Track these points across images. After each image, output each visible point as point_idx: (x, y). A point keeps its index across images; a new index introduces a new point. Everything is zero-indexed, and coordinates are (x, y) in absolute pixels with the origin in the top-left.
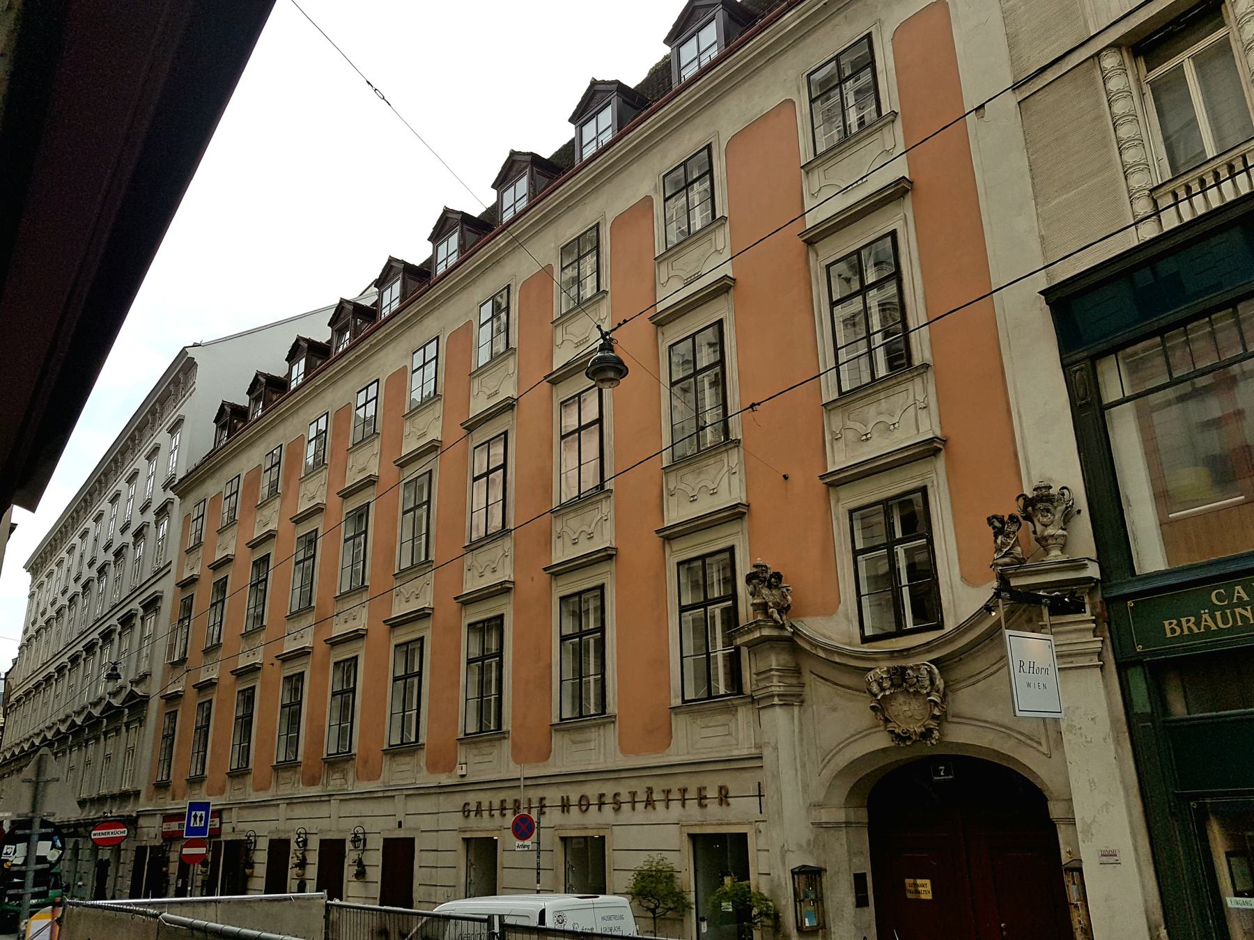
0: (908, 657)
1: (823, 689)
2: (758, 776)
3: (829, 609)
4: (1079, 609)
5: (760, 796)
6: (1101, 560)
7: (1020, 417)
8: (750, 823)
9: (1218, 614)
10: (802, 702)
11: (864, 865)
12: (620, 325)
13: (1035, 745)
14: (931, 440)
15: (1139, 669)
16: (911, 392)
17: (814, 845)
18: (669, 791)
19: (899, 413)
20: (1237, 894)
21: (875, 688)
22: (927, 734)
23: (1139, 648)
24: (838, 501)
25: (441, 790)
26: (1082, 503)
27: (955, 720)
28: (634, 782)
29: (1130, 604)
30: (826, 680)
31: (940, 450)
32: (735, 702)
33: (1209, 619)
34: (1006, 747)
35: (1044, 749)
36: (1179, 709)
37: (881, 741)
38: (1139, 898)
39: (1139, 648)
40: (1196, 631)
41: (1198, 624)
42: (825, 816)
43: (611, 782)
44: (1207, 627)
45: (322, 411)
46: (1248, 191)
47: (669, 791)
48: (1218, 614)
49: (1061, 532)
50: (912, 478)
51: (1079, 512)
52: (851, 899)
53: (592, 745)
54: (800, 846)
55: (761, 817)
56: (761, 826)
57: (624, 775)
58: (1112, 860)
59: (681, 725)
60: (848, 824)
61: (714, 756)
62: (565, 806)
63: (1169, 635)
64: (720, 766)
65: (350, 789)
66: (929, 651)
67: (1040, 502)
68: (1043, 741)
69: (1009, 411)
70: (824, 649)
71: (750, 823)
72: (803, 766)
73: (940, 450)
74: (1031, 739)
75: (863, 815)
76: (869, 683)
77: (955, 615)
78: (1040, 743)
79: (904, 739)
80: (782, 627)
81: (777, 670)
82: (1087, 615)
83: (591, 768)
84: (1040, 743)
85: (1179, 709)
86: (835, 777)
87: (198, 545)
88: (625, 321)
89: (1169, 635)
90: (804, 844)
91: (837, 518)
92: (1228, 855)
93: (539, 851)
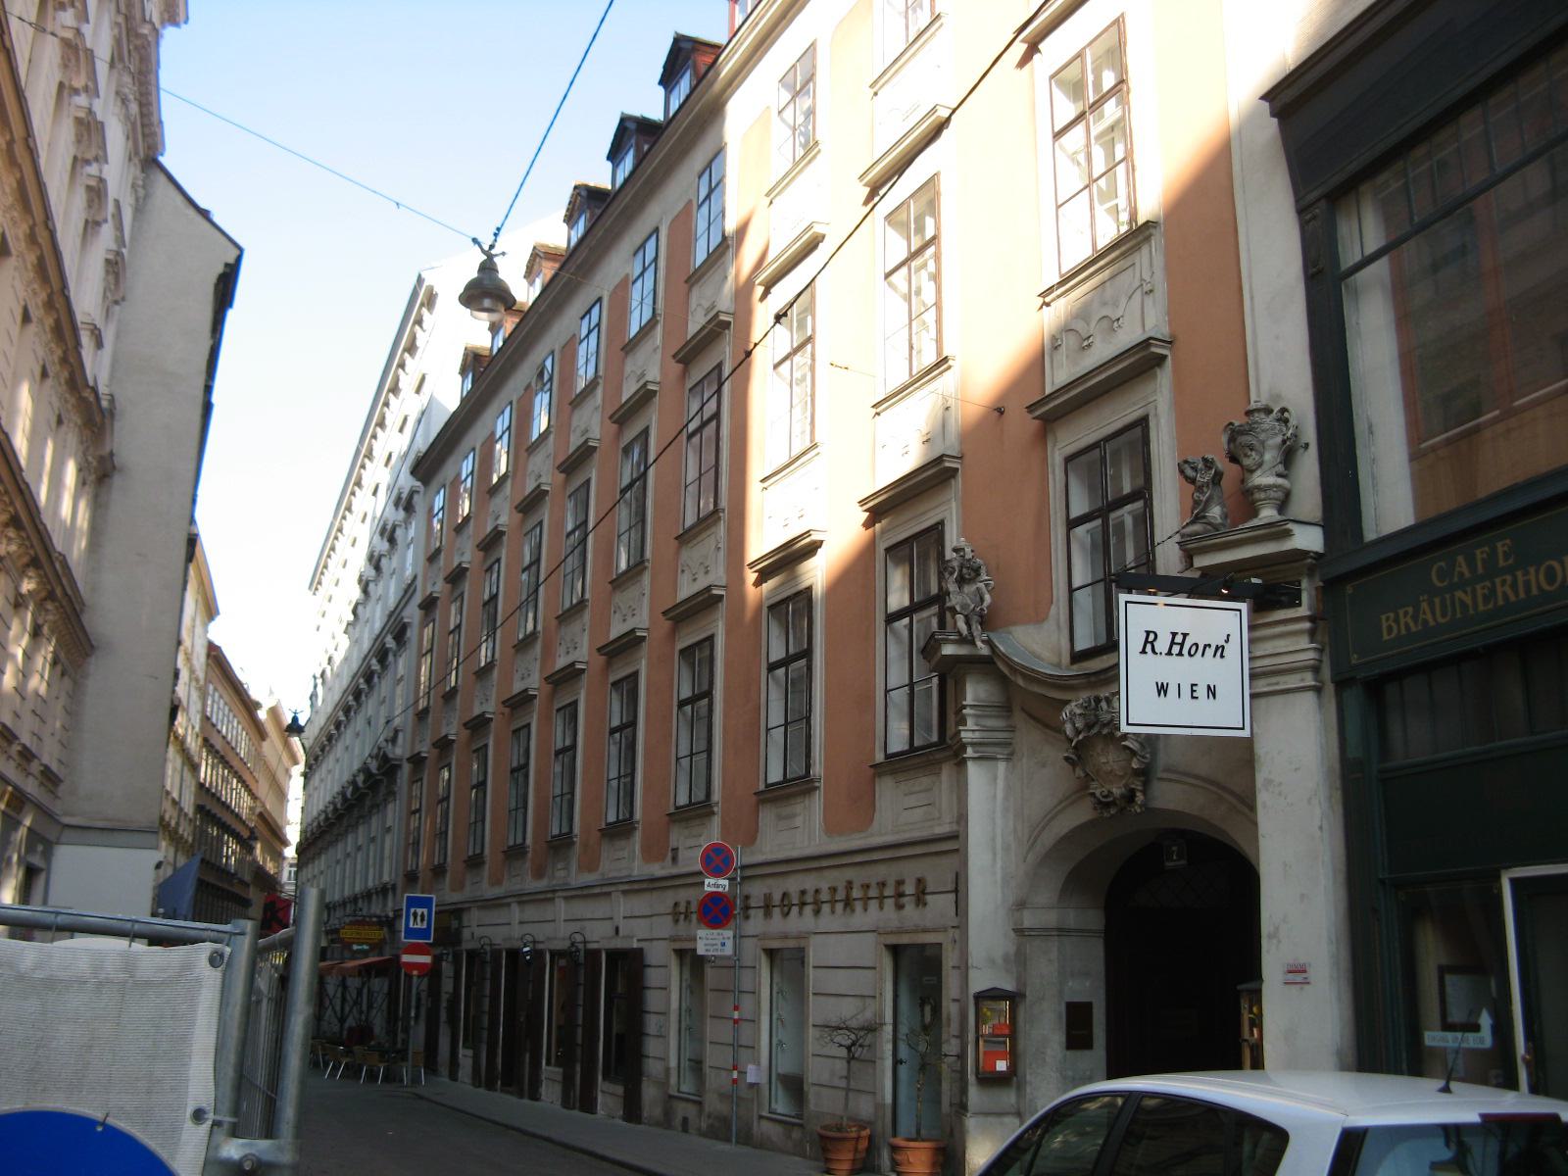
3: (1039, 618)
4: (1294, 601)
5: (956, 891)
6: (1327, 525)
7: (1252, 298)
9: (1437, 600)
11: (1090, 989)
12: (496, 235)
14: (1146, 343)
16: (1138, 265)
17: (1019, 961)
18: (868, 886)
19: (1124, 300)
20: (1448, 1027)
22: (1130, 797)
25: (653, 885)
26: (1310, 434)
28: (835, 873)
31: (1164, 357)
32: (937, 756)
33: (1428, 611)
39: (1355, 659)
40: (1414, 629)
41: (1415, 618)
42: (1029, 920)
43: (814, 875)
44: (1425, 622)
45: (547, 350)
47: (868, 886)
48: (1437, 600)
49: (1280, 481)
51: (1307, 446)
52: (1057, 1039)
53: (798, 821)
57: (825, 863)
58: (1299, 978)
59: (888, 792)
60: (1062, 931)
61: (917, 835)
62: (767, 908)
63: (1386, 637)
64: (919, 850)
65: (574, 883)
70: (1025, 676)
73: (1164, 357)
75: (1095, 919)
79: (1107, 805)
80: (970, 641)
82: (1303, 610)
83: (795, 854)
87: (637, 567)
88: (498, 229)
89: (1386, 637)
92: (1442, 971)
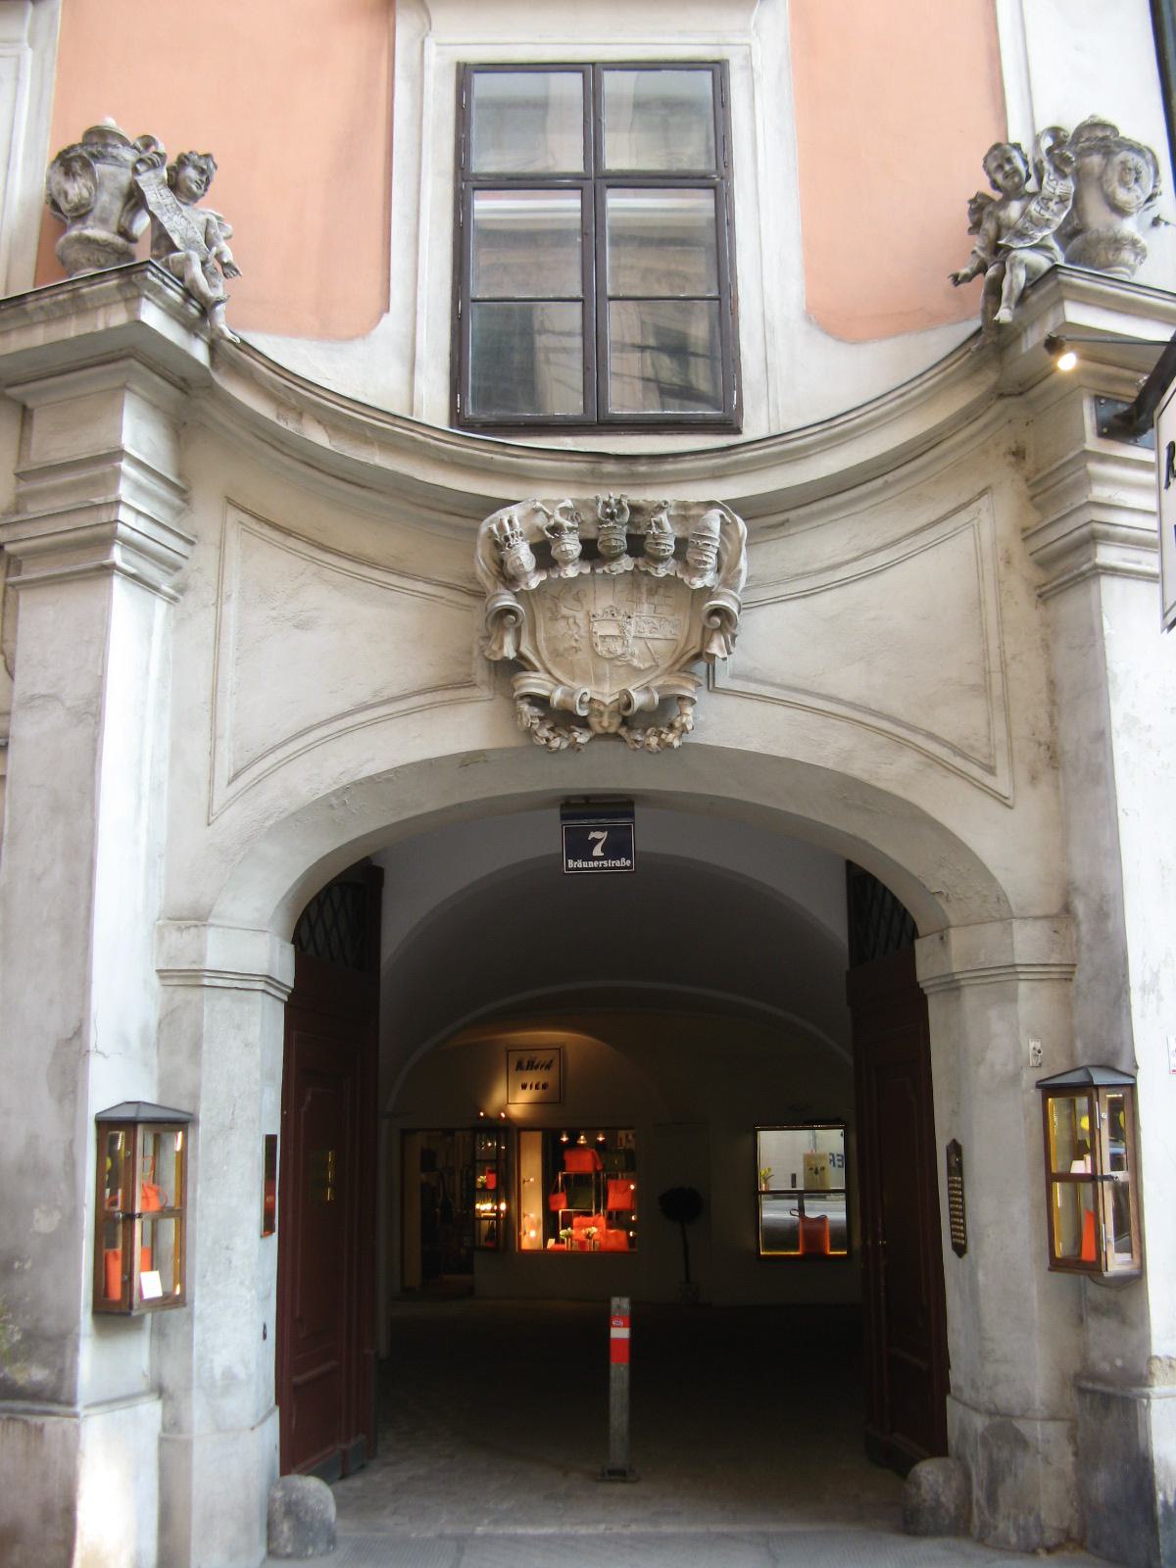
13: (976, 772)
21: (523, 555)
66: (717, 475)
74: (965, 757)
78: (991, 770)
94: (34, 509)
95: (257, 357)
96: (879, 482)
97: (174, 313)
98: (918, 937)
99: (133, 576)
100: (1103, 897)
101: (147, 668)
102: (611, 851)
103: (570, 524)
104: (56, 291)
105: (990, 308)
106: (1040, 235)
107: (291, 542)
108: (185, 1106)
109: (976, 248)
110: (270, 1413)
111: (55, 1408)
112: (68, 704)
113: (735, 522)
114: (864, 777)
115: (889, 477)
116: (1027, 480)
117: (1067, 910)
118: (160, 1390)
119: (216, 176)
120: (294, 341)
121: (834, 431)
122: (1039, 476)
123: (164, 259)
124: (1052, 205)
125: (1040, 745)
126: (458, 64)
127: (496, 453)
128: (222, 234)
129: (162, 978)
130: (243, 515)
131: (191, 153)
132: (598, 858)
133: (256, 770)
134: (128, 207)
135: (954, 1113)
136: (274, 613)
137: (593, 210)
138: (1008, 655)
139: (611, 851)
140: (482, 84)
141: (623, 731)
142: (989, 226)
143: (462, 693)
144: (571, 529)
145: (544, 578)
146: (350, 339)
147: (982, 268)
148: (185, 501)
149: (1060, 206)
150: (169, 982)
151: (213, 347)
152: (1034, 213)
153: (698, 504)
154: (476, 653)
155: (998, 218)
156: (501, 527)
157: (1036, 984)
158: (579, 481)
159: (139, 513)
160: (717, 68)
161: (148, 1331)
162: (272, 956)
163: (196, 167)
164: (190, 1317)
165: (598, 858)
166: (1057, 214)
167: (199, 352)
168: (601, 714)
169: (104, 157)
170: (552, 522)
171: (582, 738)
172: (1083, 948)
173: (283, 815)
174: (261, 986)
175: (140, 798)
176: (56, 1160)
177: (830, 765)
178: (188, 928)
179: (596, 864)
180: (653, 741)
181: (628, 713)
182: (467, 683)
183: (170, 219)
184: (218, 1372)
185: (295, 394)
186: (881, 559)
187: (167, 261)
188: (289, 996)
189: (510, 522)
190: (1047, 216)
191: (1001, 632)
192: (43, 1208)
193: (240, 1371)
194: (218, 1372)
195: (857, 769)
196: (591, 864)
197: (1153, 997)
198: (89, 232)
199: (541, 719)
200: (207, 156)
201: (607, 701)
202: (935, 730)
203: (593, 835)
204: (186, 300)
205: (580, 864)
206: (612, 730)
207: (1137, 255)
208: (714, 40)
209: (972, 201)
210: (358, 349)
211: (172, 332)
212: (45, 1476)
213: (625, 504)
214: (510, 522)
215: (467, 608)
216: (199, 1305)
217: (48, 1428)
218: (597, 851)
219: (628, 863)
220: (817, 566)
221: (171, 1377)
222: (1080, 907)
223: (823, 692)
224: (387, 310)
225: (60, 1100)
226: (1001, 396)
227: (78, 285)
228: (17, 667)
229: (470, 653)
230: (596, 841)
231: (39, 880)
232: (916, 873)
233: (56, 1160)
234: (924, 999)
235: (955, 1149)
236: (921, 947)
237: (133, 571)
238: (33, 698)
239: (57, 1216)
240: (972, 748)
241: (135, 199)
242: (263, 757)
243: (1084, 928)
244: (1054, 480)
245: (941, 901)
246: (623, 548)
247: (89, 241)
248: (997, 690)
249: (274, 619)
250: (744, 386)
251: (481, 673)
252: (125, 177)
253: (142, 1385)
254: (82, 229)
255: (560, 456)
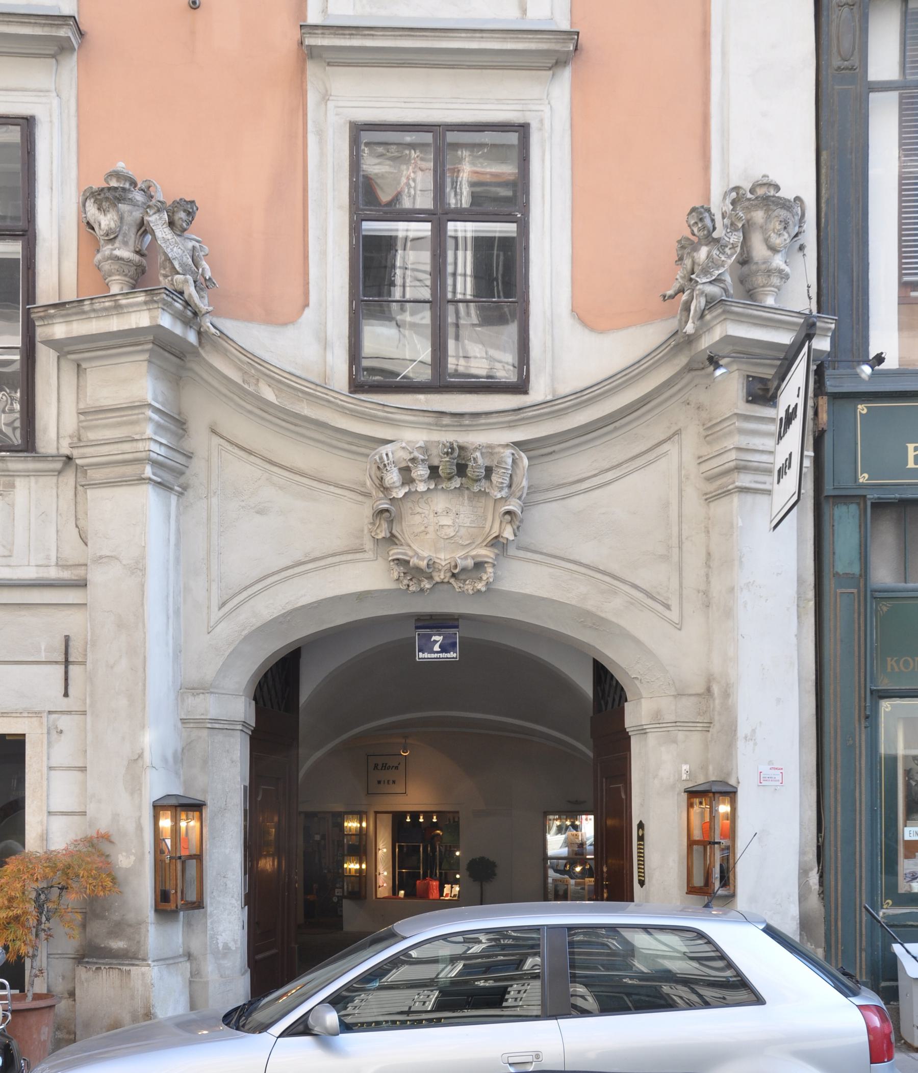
0: (468, 428)
1: (240, 469)
2: (71, 622)
7: (724, 54)
8: (38, 714)
10: (185, 488)
13: (660, 608)
15: (853, 508)
21: (393, 477)
23: (863, 478)
24: (325, 97)
27: (521, 554)
29: (862, 409)
30: (250, 452)
34: (611, 608)
35: (674, 615)
36: (884, 574)
37: (369, 576)
38: (796, 841)
39: (863, 478)
46: (363, 227)
50: (499, 101)
54: (165, 760)
55: (64, 704)
56: (64, 722)
66: (511, 425)
67: (764, 198)
68: (674, 602)
69: (706, 35)
71: (38, 714)
72: (177, 612)
74: (653, 598)
76: (381, 467)
77: (553, 378)
78: (668, 607)
81: (157, 411)
84: (668, 607)
85: (884, 574)
86: (247, 638)
90: (171, 759)
91: (320, 133)
93: (67, 663)
94: (92, 435)
95: (230, 342)
96: (611, 427)
97: (178, 316)
98: (626, 701)
99: (159, 483)
100: (728, 684)
101: (169, 539)
102: (443, 649)
103: (422, 457)
104: (103, 300)
105: (684, 319)
106: (717, 273)
107: (252, 458)
108: (199, 797)
109: (678, 277)
110: (246, 971)
111: (137, 962)
112: (124, 562)
113: (521, 457)
114: (594, 610)
115: (617, 424)
116: (704, 425)
117: (709, 690)
118: (189, 956)
119: (198, 215)
120: (250, 325)
121: (584, 397)
122: (710, 424)
123: (170, 278)
124: (727, 250)
125: (699, 592)
126: (350, 122)
127: (379, 410)
128: (202, 254)
129: (183, 723)
130: (221, 440)
131: (181, 199)
132: (437, 652)
133: (236, 601)
134: (140, 232)
135: (642, 805)
136: (243, 504)
137: (439, 233)
138: (684, 537)
139: (443, 649)
140: (366, 136)
141: (452, 581)
142: (688, 262)
143: (358, 556)
144: (423, 460)
145: (407, 490)
146: (285, 324)
147: (681, 291)
148: (184, 430)
149: (733, 250)
150: (188, 726)
151: (199, 333)
152: (715, 256)
153: (500, 445)
154: (366, 531)
155: (693, 257)
156: (381, 458)
157: (687, 733)
158: (428, 427)
159: (161, 444)
160: (523, 129)
161: (181, 923)
162: (241, 709)
163: (185, 211)
164: (205, 914)
165: (437, 652)
166: (729, 257)
167: (192, 337)
168: (440, 570)
169: (124, 199)
170: (412, 456)
171: (427, 585)
172: (716, 713)
173: (253, 628)
174: (240, 727)
175: (168, 618)
176: (131, 827)
177: (574, 603)
178: (198, 694)
179: (436, 655)
180: (470, 587)
181: (456, 571)
182: (360, 550)
183: (172, 250)
184: (221, 946)
185: (255, 365)
186: (610, 476)
187: (172, 280)
188: (252, 731)
189: (387, 455)
190: (723, 259)
191: (680, 523)
192: (124, 854)
193: (232, 946)
194: (221, 946)
195: (590, 605)
196: (433, 656)
197: (751, 743)
198: (117, 253)
199: (404, 573)
200: (193, 202)
201: (443, 563)
202: (638, 582)
203: (434, 638)
204: (185, 307)
205: (426, 655)
206: (446, 580)
207: (782, 278)
208: (519, 107)
209: (679, 242)
210: (290, 331)
211: (178, 329)
212: (132, 998)
213: (455, 446)
214: (387, 455)
215: (361, 503)
216: (209, 909)
217: (132, 973)
218: (437, 648)
219: (455, 655)
220: (571, 480)
221: (195, 946)
222: (716, 689)
223: (571, 558)
224: (306, 305)
225: (132, 794)
226: (691, 370)
227: (118, 298)
228: (89, 537)
229: (363, 531)
230: (436, 642)
231: (112, 667)
232: (624, 666)
233: (131, 827)
234: (629, 737)
235: (641, 826)
236: (628, 707)
237: (159, 480)
238: (101, 557)
239: (133, 858)
240: (658, 593)
241: (143, 228)
242: (240, 592)
243: (717, 702)
244: (718, 429)
245: (637, 682)
246: (457, 469)
247: (119, 259)
248: (675, 558)
249: (243, 507)
250: (531, 362)
251: (369, 545)
252: (137, 214)
253: (181, 951)
254: (113, 250)
255: (417, 413)
